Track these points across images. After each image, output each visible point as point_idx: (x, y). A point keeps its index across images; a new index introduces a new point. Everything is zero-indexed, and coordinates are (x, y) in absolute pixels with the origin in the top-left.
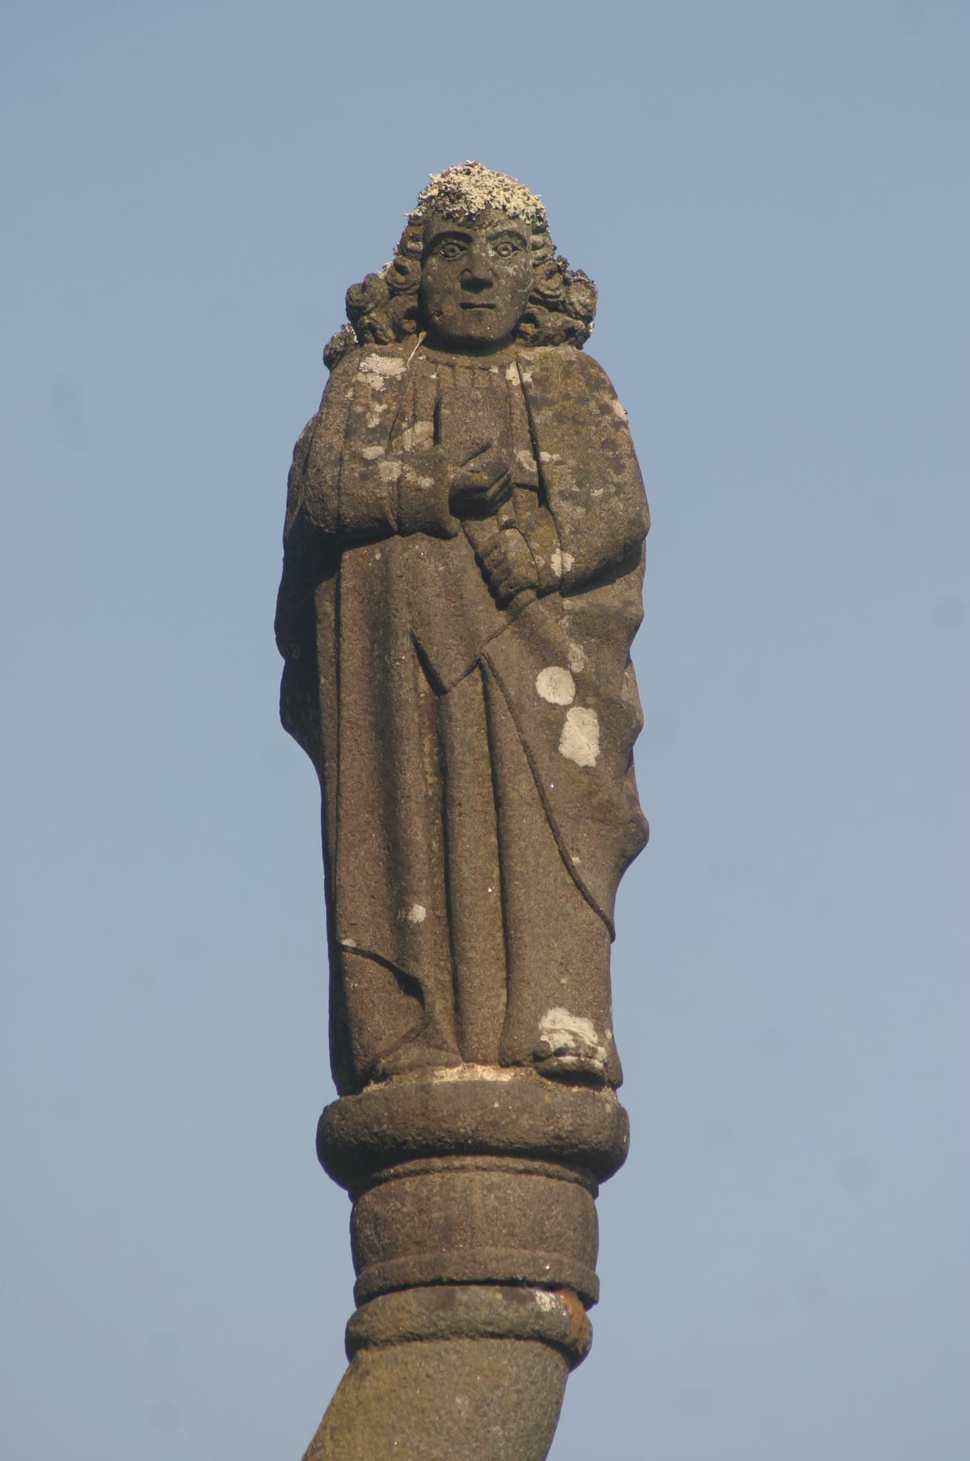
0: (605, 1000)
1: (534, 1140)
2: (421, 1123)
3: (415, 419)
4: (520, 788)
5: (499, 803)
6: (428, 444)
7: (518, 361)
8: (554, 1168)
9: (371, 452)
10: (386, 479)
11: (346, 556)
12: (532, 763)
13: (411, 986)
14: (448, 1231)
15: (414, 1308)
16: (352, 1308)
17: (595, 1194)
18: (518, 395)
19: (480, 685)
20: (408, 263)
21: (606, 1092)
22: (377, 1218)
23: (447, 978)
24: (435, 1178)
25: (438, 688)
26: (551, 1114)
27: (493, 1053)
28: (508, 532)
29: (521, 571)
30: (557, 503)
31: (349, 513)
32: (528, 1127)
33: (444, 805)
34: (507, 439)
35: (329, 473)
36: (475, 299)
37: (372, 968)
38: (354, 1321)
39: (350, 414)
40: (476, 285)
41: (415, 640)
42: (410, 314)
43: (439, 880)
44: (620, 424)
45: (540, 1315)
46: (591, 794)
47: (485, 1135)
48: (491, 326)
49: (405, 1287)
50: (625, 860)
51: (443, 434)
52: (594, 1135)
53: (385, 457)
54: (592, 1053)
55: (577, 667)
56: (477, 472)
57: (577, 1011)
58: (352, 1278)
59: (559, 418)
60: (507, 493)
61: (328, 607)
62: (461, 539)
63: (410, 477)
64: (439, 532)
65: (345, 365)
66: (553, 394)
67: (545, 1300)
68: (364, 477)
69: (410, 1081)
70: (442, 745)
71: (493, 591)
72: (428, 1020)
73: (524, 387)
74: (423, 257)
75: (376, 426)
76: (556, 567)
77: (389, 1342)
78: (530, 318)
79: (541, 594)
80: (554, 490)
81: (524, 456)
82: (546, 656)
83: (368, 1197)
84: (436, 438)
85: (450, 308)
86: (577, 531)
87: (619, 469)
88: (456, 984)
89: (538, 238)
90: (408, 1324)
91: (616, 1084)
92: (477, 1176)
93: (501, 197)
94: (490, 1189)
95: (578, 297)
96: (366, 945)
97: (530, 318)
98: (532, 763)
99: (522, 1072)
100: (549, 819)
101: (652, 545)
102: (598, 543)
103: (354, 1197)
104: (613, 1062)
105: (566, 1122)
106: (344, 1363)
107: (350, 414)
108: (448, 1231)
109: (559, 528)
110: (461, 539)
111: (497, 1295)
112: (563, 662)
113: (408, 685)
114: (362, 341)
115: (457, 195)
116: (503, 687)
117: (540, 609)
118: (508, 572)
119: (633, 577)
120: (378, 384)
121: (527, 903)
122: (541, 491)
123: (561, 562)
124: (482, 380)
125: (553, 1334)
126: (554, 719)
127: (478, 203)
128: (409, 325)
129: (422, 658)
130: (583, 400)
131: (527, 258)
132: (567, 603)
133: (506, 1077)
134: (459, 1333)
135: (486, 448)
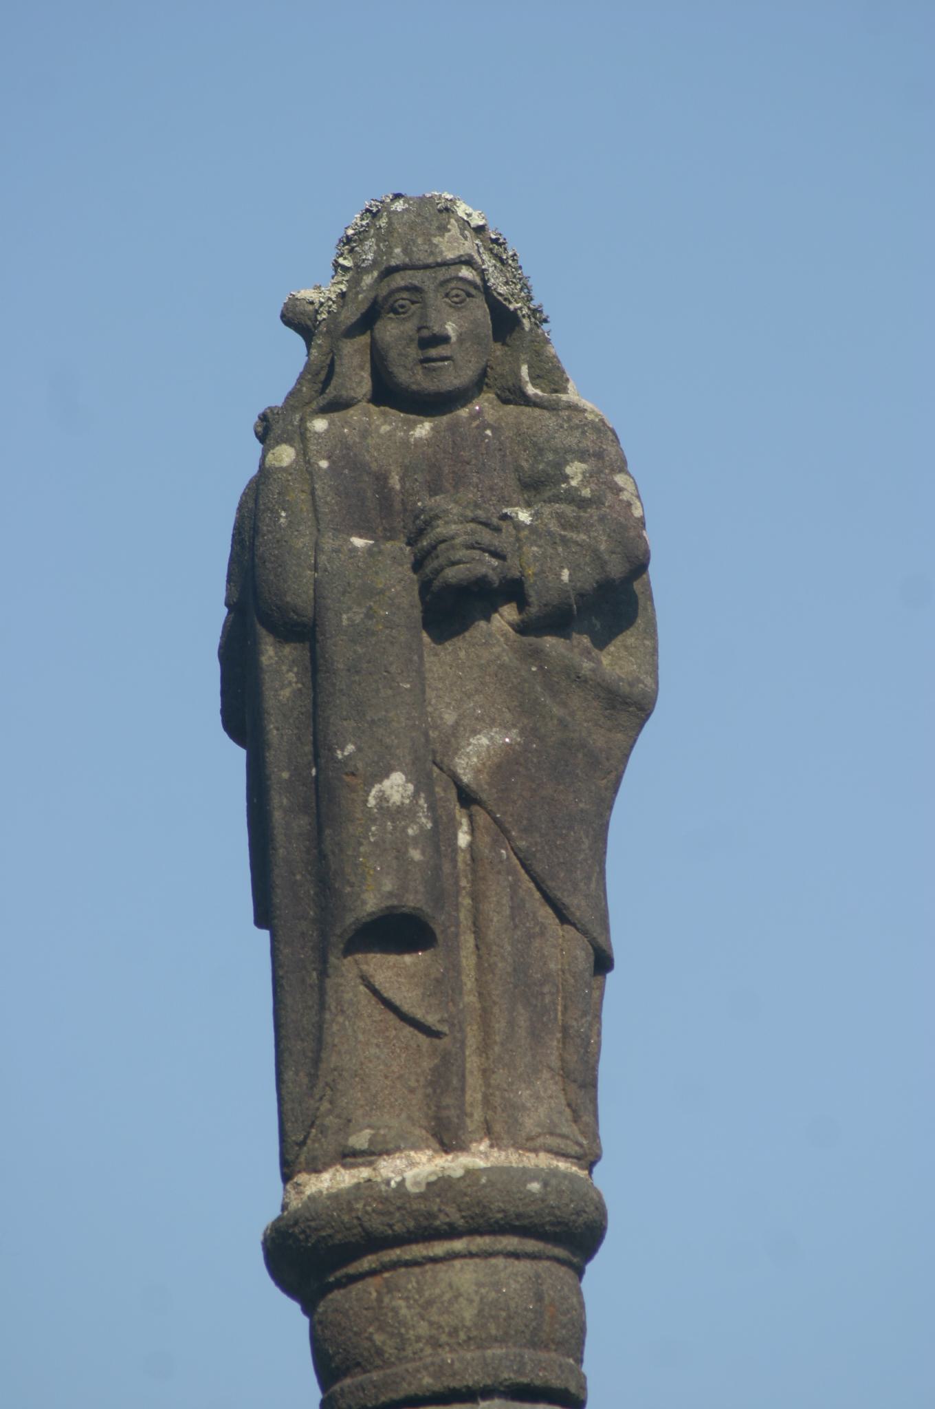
17: (580, 1272)
103: (308, 1309)
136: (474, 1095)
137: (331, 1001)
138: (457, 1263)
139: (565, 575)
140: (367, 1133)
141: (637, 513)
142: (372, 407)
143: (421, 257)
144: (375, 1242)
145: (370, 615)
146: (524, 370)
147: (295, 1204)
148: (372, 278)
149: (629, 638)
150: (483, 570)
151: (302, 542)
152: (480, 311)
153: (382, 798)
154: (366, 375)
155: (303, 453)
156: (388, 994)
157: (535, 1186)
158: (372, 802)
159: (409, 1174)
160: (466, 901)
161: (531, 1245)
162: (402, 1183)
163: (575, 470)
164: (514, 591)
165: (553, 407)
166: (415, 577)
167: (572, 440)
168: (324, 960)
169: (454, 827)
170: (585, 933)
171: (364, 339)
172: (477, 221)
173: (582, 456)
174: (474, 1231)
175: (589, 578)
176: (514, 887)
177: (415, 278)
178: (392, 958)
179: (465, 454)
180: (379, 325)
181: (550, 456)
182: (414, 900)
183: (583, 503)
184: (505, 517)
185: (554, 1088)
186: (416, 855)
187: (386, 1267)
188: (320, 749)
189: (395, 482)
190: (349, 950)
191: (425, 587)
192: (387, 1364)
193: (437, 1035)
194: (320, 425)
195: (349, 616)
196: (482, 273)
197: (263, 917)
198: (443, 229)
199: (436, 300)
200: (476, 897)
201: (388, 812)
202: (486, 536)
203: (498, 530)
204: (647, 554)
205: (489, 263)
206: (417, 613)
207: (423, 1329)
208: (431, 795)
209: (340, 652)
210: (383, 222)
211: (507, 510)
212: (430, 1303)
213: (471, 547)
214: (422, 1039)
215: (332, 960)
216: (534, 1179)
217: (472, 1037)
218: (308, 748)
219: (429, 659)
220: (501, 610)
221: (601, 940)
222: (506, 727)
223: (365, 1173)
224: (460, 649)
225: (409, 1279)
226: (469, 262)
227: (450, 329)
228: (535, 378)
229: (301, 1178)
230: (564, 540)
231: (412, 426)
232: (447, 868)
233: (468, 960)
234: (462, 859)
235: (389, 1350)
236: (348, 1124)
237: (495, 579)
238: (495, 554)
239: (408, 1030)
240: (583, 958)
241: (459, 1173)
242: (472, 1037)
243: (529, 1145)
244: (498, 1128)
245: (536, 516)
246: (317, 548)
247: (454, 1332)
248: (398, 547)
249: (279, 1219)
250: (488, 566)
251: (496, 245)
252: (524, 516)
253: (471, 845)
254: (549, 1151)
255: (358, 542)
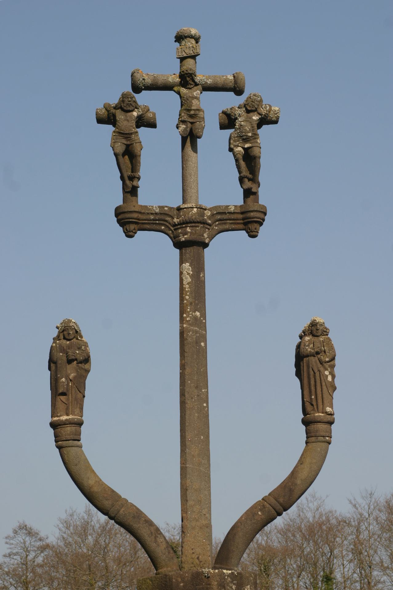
0: (333, 406)
1: (326, 421)
2: (314, 419)
3: (311, 344)
4: (324, 384)
5: (321, 385)
6: (313, 347)
7: (322, 338)
8: (328, 424)
9: (307, 348)
10: (309, 350)
11: (304, 359)
12: (325, 381)
13: (312, 405)
14: (317, 431)
15: (314, 439)
16: (306, 439)
17: (81, 427)
18: (322, 341)
19: (319, 373)
20: (310, 327)
21: (333, 416)
22: (309, 430)
23: (316, 404)
24: (315, 425)
25: (314, 373)
26: (328, 418)
27: (321, 412)
28: (322, 356)
29: (323, 361)
30: (326, 353)
31: (305, 354)
32: (325, 420)
33: (315, 385)
34: (321, 347)
35: (303, 350)
36: (317, 331)
37: (308, 403)
38: (306, 440)
39: (304, 344)
40: (317, 330)
41: (312, 368)
42: (310, 333)
43: (315, 394)
44: (333, 344)
45: (327, 440)
46: (331, 384)
47: (321, 421)
48: (319, 334)
49: (312, 437)
50: (334, 391)
51: (314, 346)
52: (332, 421)
53: (308, 348)
54: (332, 412)
55: (329, 371)
57: (330, 407)
58: (306, 436)
59: (326, 344)
60: (321, 352)
61: (302, 364)
62: (316, 357)
63: (311, 350)
65: (303, 339)
66: (326, 341)
67: (327, 438)
68: (306, 350)
69: (312, 415)
70: (315, 379)
71: (320, 362)
72: (314, 408)
73: (322, 341)
74: (312, 327)
75: (200, 315)
76: (327, 360)
77: (311, 443)
78: (323, 333)
79: (325, 363)
80: (326, 352)
81: (323, 348)
83: (308, 427)
84: (314, 346)
85: (315, 332)
86: (329, 356)
87: (333, 349)
88: (317, 405)
89: (324, 325)
90: (313, 441)
91: (334, 415)
92: (320, 425)
93: (320, 321)
94: (321, 426)
95: (328, 331)
96: (307, 400)
97: (323, 333)
98: (325, 381)
99: (324, 414)
100: (327, 387)
101: (336, 358)
102: (331, 357)
103: (54, 430)
104: (334, 413)
105: (329, 419)
106: (305, 445)
107: (304, 344)
108: (317, 431)
109: (327, 356)
110: (316, 357)
111: (322, 438)
112: (327, 370)
113: (311, 373)
114: (305, 336)
115: (315, 320)
116: (322, 373)
117: (325, 364)
118: (322, 361)
119: (334, 361)
120: (307, 340)
121: (325, 396)
122: (325, 352)
123: (327, 359)
124: (318, 340)
125: (328, 442)
126: (327, 376)
127: (318, 321)
128: (310, 334)
129: (313, 370)
130: (329, 342)
131: (322, 327)
132: (328, 364)
133: (323, 415)
134: (318, 442)
135: (319, 347)
136: (70, 410)
137: (56, 401)
138: (68, 427)
139: (81, 358)
140: (59, 414)
141: (89, 351)
142: (63, 340)
143: (68, 326)
144: (60, 425)
145: (62, 362)
146: (78, 337)
147: (52, 421)
149: (88, 364)
150: (73, 358)
151: (55, 354)
152: (74, 331)
153: (62, 381)
154: (63, 337)
155: (56, 344)
156: (62, 400)
157: (76, 420)
158: (61, 381)
159: (63, 418)
160: (70, 391)
161: (75, 425)
162: (62, 420)
163: (83, 347)
164: (76, 360)
165: (81, 340)
167: (83, 344)
168: (56, 396)
169: (69, 383)
170: (82, 394)
171: (63, 333)
172: (74, 322)
173: (84, 346)
174: (69, 424)
175: (84, 358)
176: (75, 389)
177: (67, 328)
178: (63, 396)
179: (72, 345)
180: (64, 332)
181: (81, 346)
182: (65, 391)
183: (84, 351)
184: (76, 352)
185: (79, 409)
186: (65, 386)
187: (61, 427)
189: (65, 348)
190: (58, 396)
191: (67, 359)
192: (61, 437)
193: (67, 404)
194: (58, 342)
196: (74, 327)
197: (51, 390)
198: (71, 323)
199: (70, 330)
200: (71, 390)
201: (63, 382)
202: (73, 354)
203: (75, 354)
204: (90, 356)
205: (75, 326)
206: (66, 362)
207: (64, 434)
208: (67, 380)
209: (59, 366)
210: (65, 322)
211: (76, 351)
212: (65, 431)
213: (72, 355)
214: (65, 405)
215: (57, 396)
216: (76, 419)
217: (70, 404)
218: (55, 375)
219: (67, 366)
221: (84, 394)
222: (75, 373)
223: (59, 418)
224: (70, 365)
225: (63, 429)
226: (73, 326)
227: (71, 333)
228: (80, 337)
229: (53, 418)
230: (81, 355)
231: (67, 342)
232: (68, 387)
233: (70, 397)
234: (70, 387)
235: (61, 436)
236: (58, 413)
237: (74, 359)
238: (75, 356)
239: (64, 404)
240: (82, 396)
241: (68, 419)
242: (70, 404)
243: (76, 415)
244: (73, 414)
245: (79, 352)
246: (57, 355)
247: (67, 434)
248: (65, 355)
249: (51, 422)
250: (74, 357)
251: (76, 324)
252: (78, 352)
253: (71, 385)
254: (78, 416)
255: (61, 354)
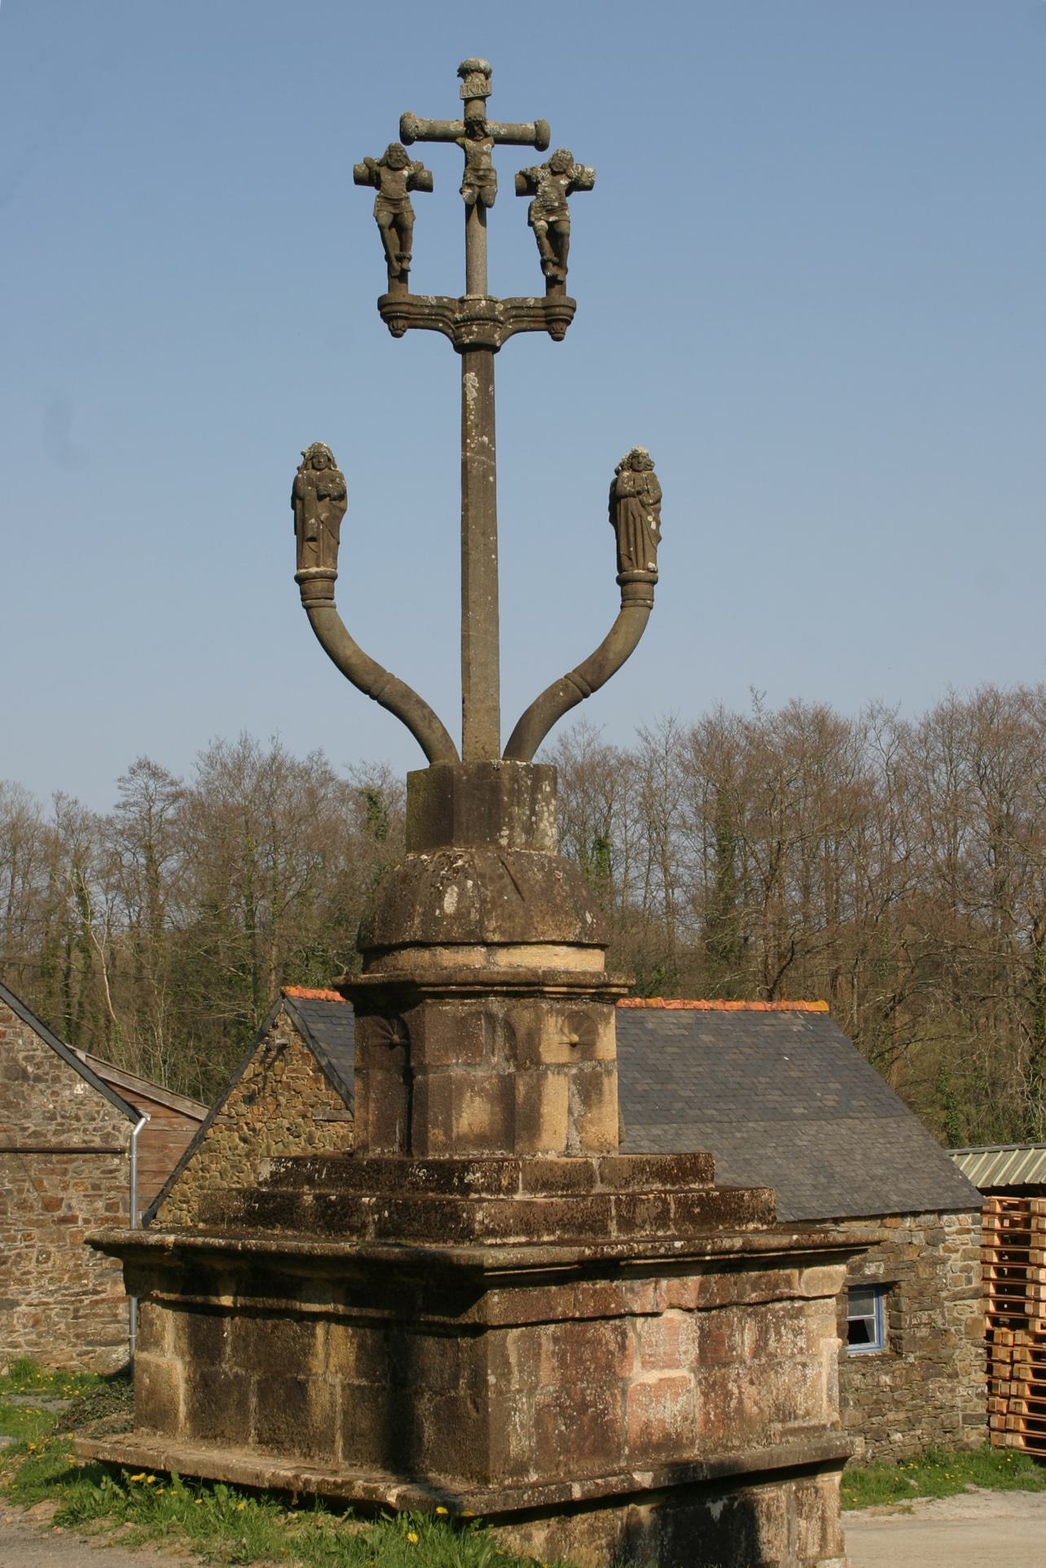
4: (646, 532)
13: (630, 559)
32: (647, 578)
33: (635, 534)
56: (639, 489)
64: (634, 497)
70: (635, 525)
82: (207, 1162)
122: (648, 492)
123: (651, 501)
126: (650, 523)
148: (596, 1284)
164: (329, 495)
166: (776, 715)
188: (304, 515)
195: (308, 498)
197: (296, 533)
209: (306, 502)
220: (1017, 1331)
224: (322, 503)
248: (315, 489)
